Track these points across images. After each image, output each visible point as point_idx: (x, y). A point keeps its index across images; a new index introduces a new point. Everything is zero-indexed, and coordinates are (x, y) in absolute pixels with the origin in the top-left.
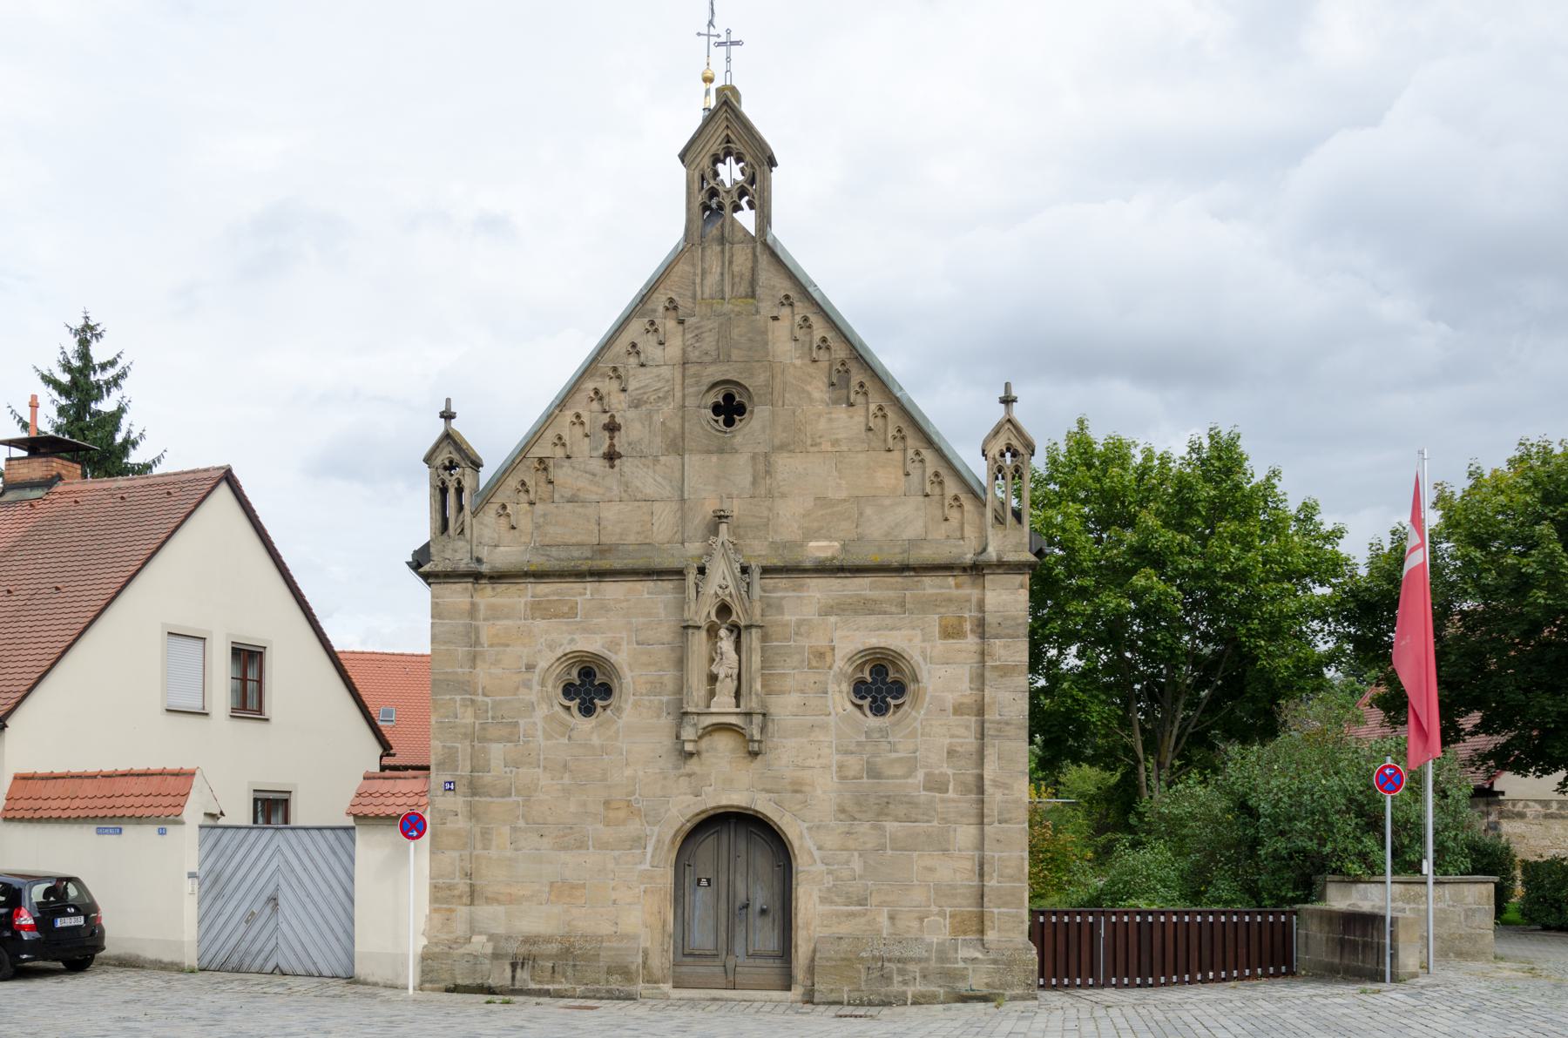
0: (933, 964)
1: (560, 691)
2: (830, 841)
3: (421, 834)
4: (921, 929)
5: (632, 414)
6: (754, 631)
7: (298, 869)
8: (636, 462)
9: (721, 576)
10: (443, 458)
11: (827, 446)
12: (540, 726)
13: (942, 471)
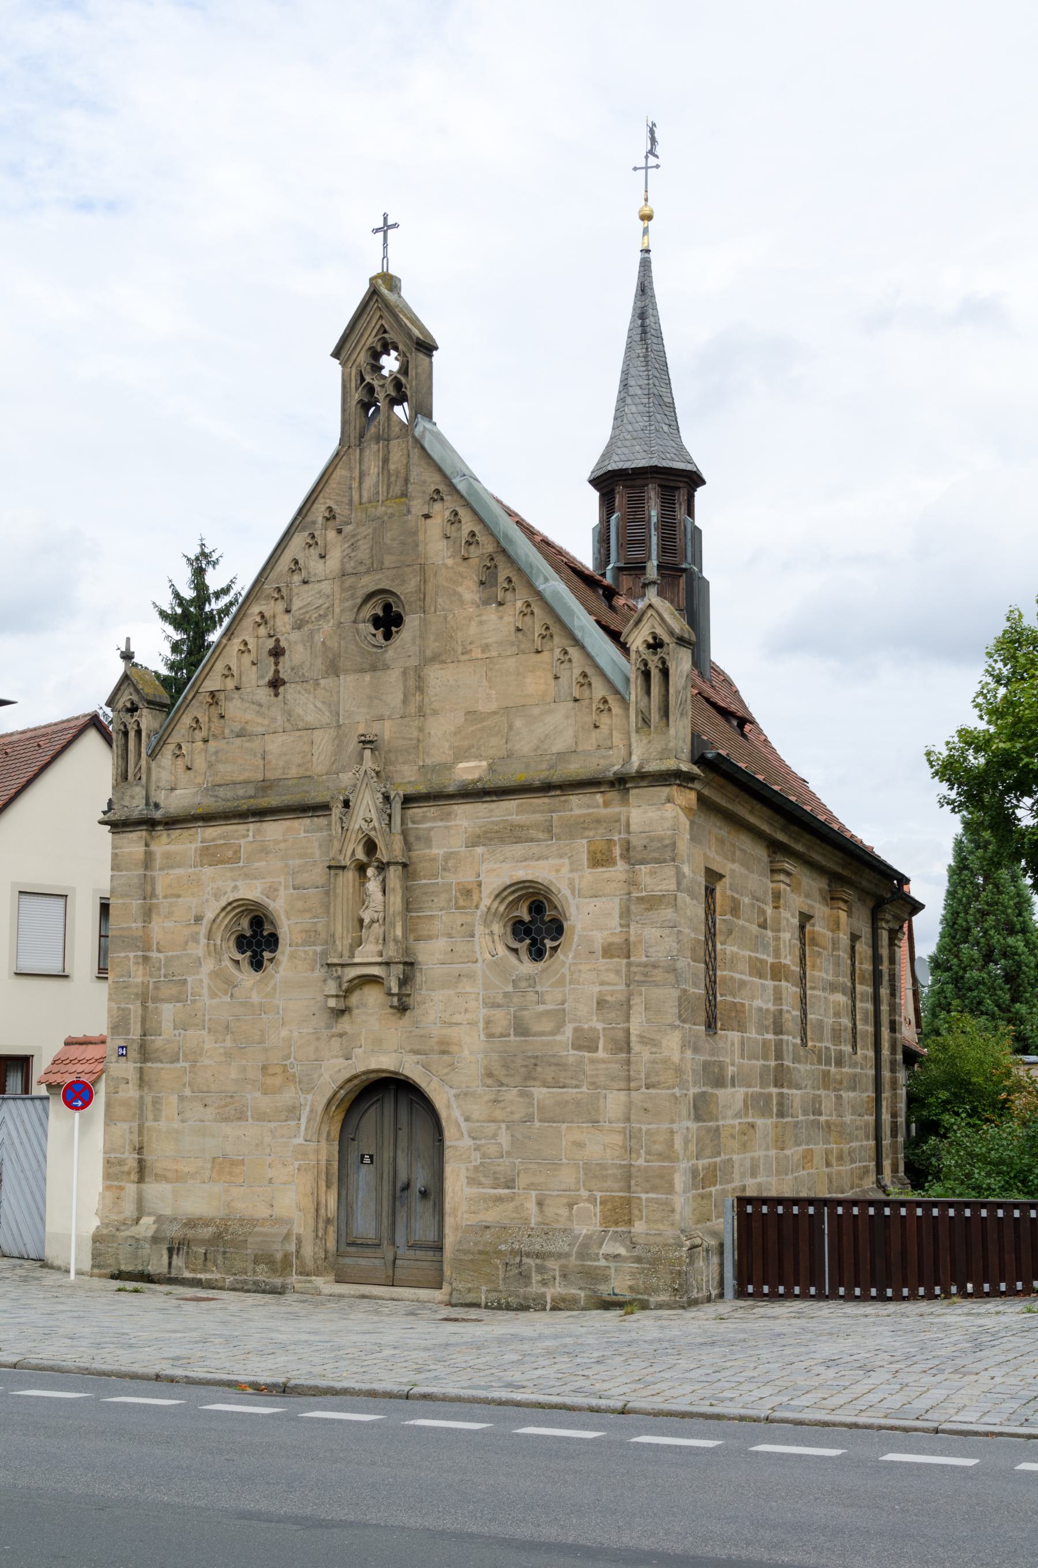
0: (573, 1261)
1: (232, 944)
2: (478, 1110)
4: (570, 1219)
5: (295, 636)
6: (392, 868)
7: (17, 1142)
8: (299, 688)
9: (367, 806)
10: (124, 700)
11: (477, 653)
12: (205, 984)
13: (590, 671)
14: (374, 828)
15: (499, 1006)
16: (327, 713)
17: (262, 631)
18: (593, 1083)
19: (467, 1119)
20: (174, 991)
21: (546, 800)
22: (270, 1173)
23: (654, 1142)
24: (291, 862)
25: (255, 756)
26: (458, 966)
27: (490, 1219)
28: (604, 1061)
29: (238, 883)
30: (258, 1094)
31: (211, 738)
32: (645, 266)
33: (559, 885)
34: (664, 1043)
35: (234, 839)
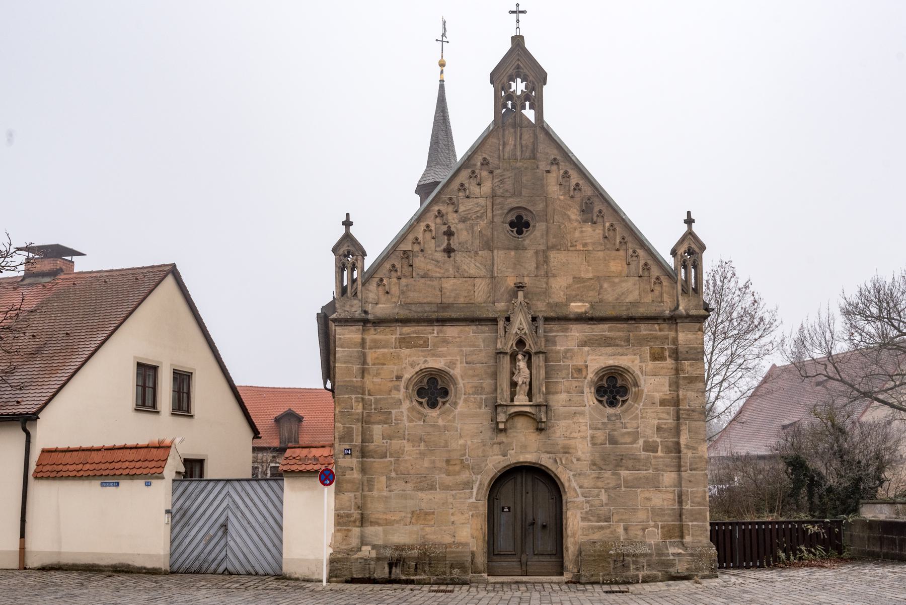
4: (644, 536)
5: (461, 226)
8: (464, 254)
9: (521, 322)
14: (525, 334)
19: (581, 487)
20: (382, 417)
21: (626, 326)
25: (435, 289)
28: (661, 457)
30: (444, 476)
32: (442, 87)
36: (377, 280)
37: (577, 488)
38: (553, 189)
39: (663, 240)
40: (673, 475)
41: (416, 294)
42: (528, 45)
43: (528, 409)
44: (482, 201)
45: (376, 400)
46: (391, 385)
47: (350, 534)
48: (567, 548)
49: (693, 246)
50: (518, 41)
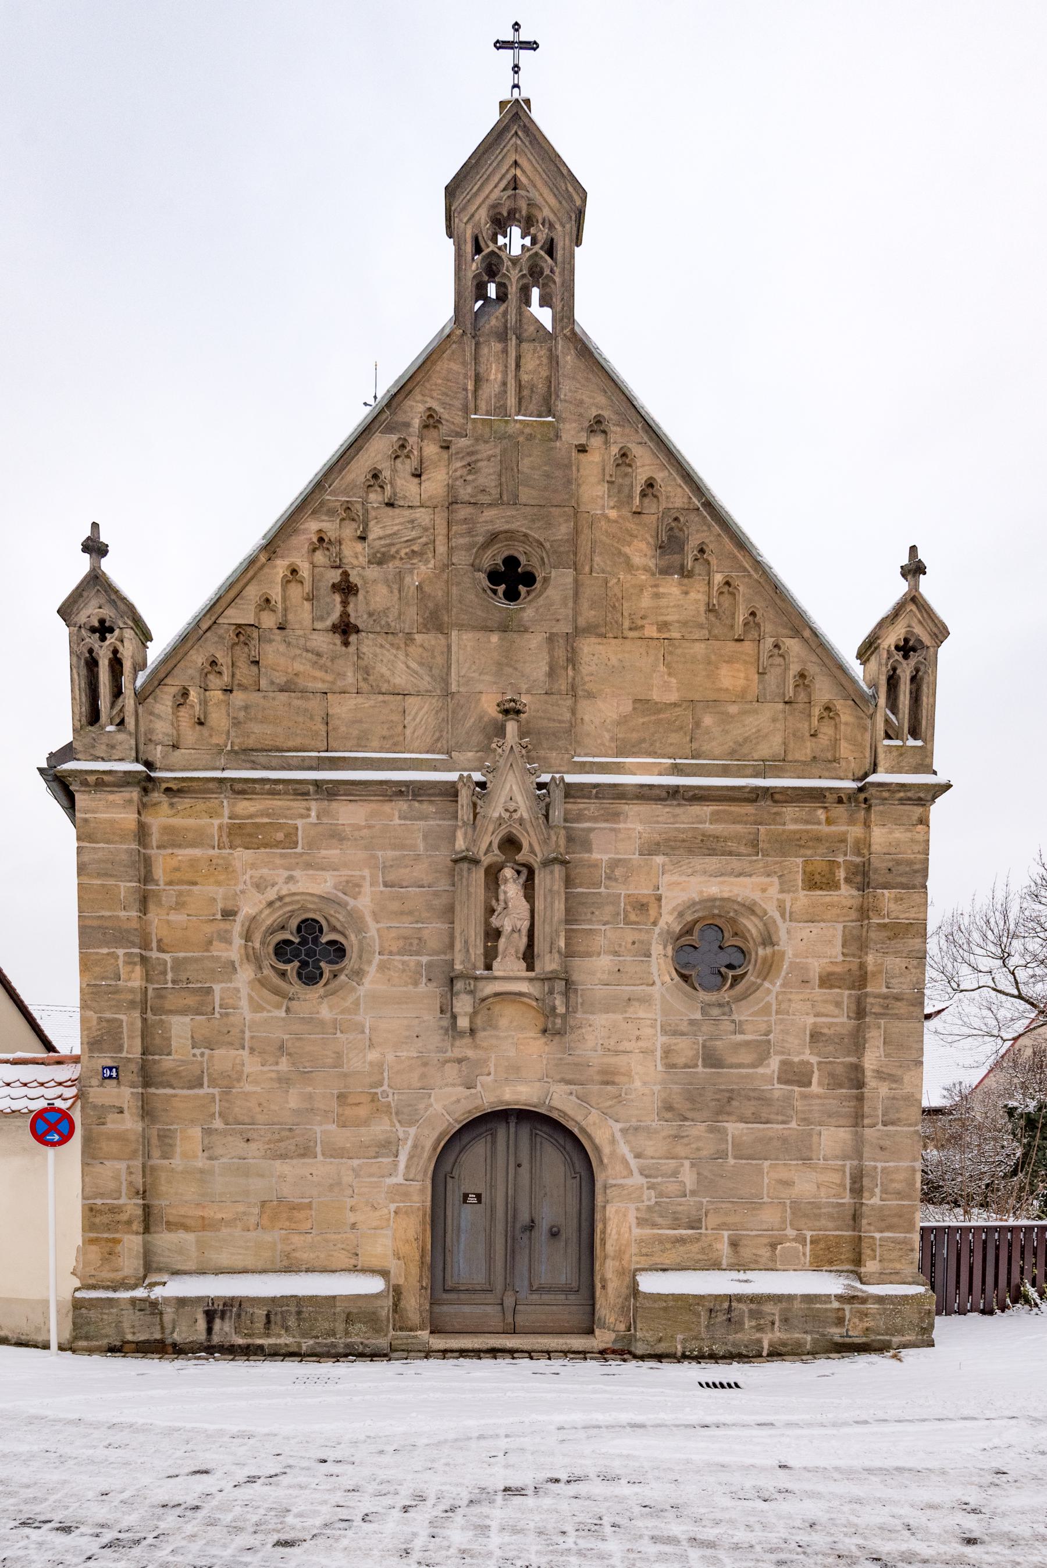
2: (652, 1147)
3: (65, 1139)
5: (373, 572)
8: (380, 640)
15: (683, 1034)
16: (427, 678)
17: (320, 557)
18: (804, 1119)
19: (638, 1156)
20: (191, 1001)
22: (352, 1218)
23: (892, 1181)
24: (380, 853)
25: (312, 718)
26: (627, 988)
27: (667, 1261)
28: (818, 1097)
29: (294, 873)
30: (333, 1127)
31: (235, 688)
33: (764, 906)
34: (906, 1079)
35: (286, 817)
36: (173, 690)
37: (630, 1157)
38: (594, 493)
39: (846, 612)
40: (844, 1134)
41: (269, 729)
42: (538, 115)
43: (524, 987)
44: (423, 516)
45: (175, 960)
46: (208, 929)
47: (119, 1248)
48: (603, 1280)
49: (918, 630)
50: (516, 117)
